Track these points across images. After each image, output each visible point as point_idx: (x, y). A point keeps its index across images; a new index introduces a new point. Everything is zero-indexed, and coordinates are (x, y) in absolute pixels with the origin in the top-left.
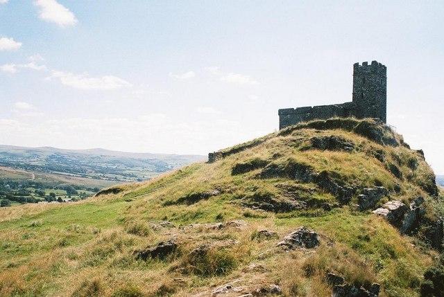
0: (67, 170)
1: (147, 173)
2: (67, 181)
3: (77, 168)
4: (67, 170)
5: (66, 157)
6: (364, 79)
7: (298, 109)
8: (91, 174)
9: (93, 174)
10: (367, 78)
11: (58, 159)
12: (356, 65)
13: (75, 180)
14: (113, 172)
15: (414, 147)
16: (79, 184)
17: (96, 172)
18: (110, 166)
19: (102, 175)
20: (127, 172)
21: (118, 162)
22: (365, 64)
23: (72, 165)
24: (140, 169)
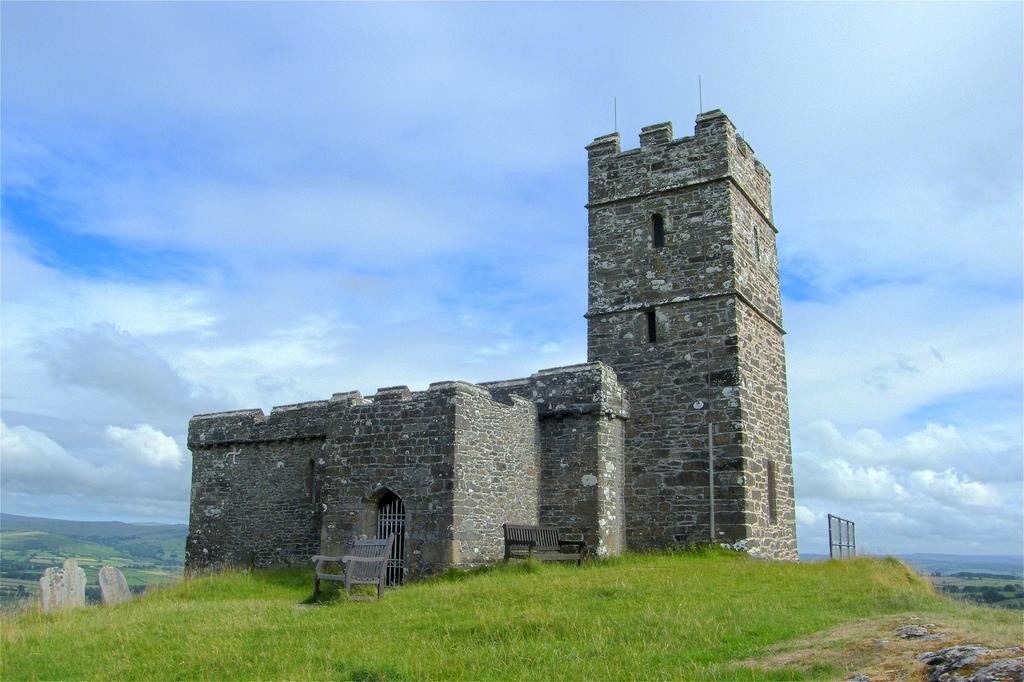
12: (601, 151)
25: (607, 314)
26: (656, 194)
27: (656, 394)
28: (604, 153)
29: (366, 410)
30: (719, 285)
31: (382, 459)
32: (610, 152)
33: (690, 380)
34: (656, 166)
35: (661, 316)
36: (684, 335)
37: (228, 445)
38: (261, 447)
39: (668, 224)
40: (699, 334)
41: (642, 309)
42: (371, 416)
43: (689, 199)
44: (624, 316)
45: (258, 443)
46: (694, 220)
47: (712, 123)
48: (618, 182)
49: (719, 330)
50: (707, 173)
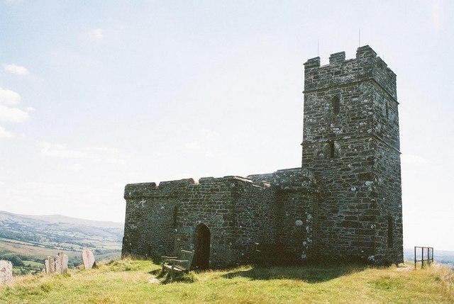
0: (18, 237)
1: (107, 244)
2: (15, 250)
3: (31, 235)
4: (18, 237)
5: (20, 222)
6: (336, 100)
7: (163, 185)
8: (44, 243)
9: (47, 243)
10: (347, 97)
11: (11, 225)
12: (312, 66)
13: (24, 250)
14: (70, 241)
15: (401, 151)
16: (27, 254)
17: (50, 241)
18: (68, 234)
19: (57, 244)
20: (85, 241)
21: (77, 230)
22: (338, 58)
23: (25, 232)
24: (101, 239)
34: (337, 73)
39: (342, 101)
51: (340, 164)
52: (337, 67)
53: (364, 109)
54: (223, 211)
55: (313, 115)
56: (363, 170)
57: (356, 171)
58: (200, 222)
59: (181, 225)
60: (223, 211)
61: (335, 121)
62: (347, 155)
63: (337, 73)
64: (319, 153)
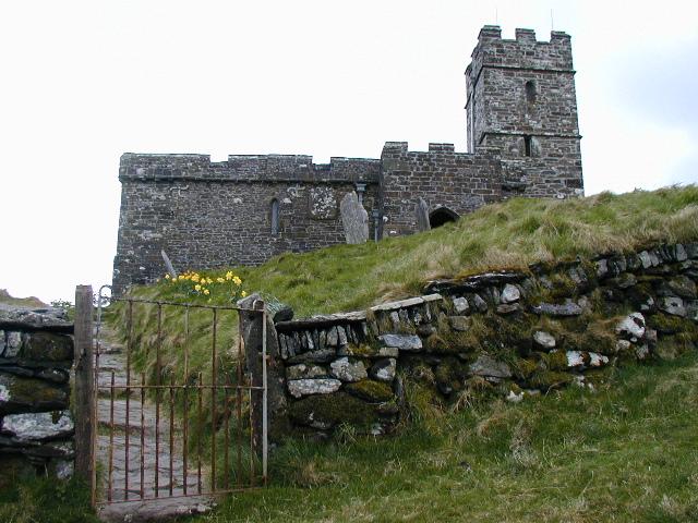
10: (544, 86)
12: (489, 34)
25: (501, 135)
26: (529, 70)
27: (534, 187)
28: (493, 36)
29: (421, 156)
30: (571, 131)
31: (440, 189)
32: (496, 36)
33: (555, 182)
34: (529, 54)
35: (535, 141)
36: (550, 155)
37: (172, 181)
38: (213, 185)
39: (538, 90)
40: (560, 156)
41: (524, 135)
42: (428, 160)
43: (550, 78)
44: (511, 138)
45: (212, 181)
46: (554, 91)
47: (561, 38)
48: (505, 56)
49: (572, 156)
50: (561, 66)
51: (542, 165)
52: (530, 46)
53: (567, 105)
54: (485, 192)
55: (499, 98)
56: (569, 176)
57: (563, 176)
58: (439, 205)
59: (396, 210)
60: (485, 192)
61: (530, 111)
62: (550, 155)
63: (529, 54)
64: (511, 148)
